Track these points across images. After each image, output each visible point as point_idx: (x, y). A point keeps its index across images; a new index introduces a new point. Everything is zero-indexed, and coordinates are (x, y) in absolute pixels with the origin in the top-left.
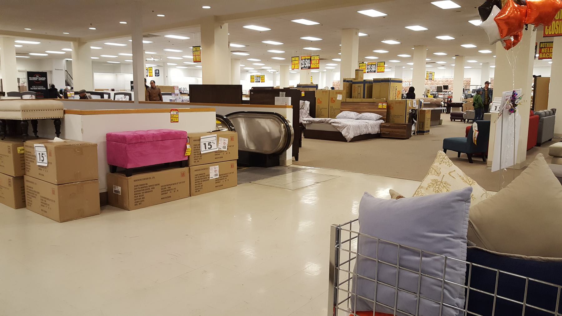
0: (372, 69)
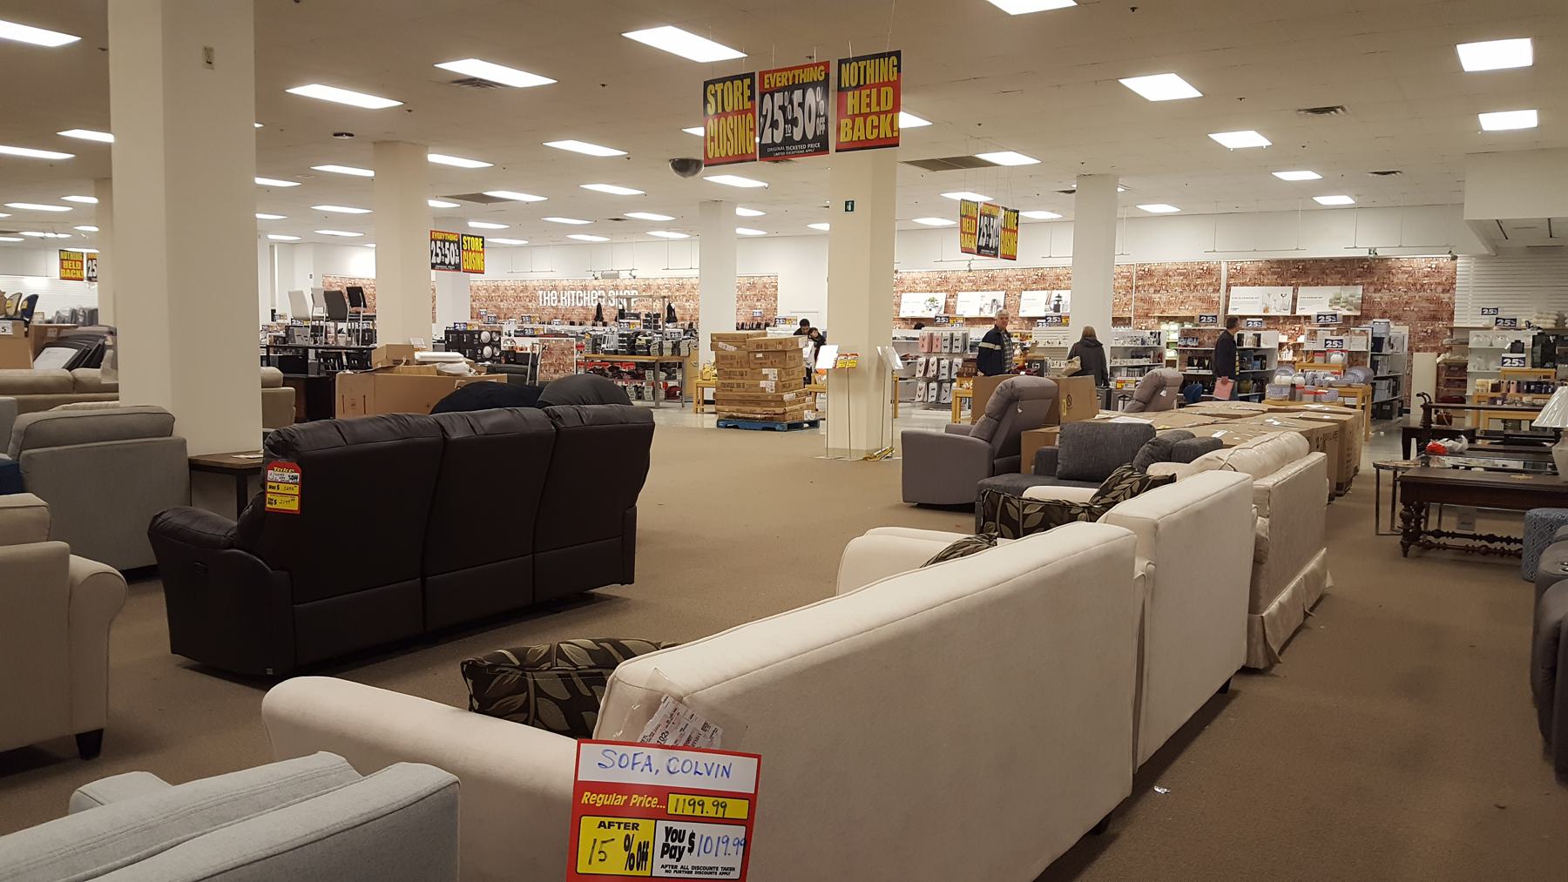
0: (446, 256)
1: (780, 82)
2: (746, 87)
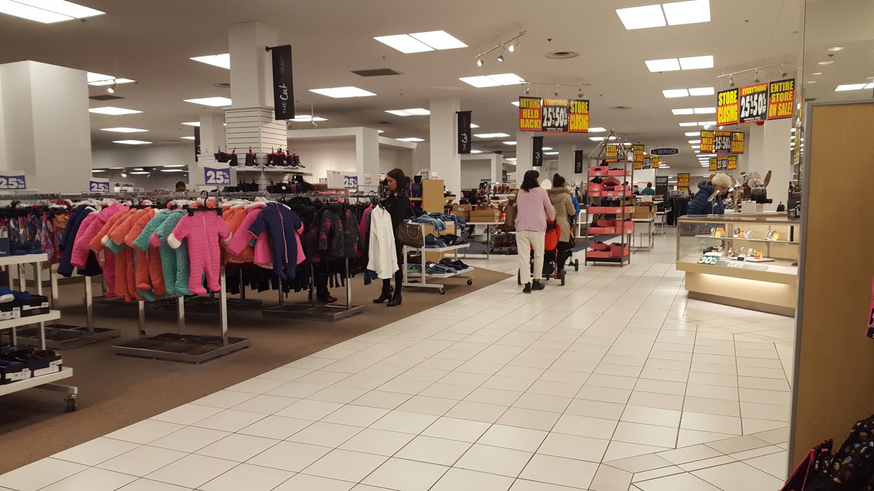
1: (774, 90)
2: (735, 94)
